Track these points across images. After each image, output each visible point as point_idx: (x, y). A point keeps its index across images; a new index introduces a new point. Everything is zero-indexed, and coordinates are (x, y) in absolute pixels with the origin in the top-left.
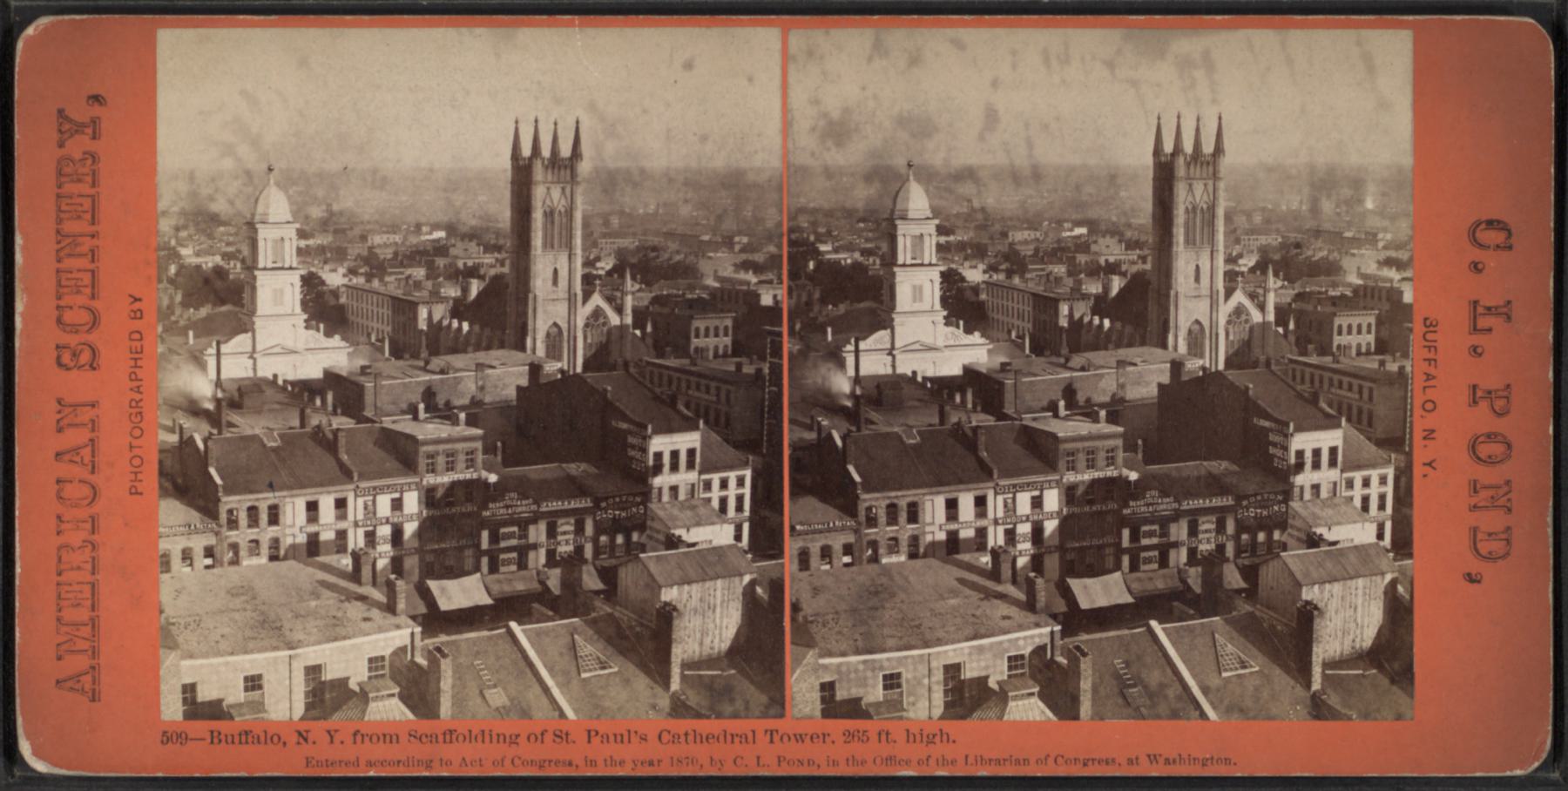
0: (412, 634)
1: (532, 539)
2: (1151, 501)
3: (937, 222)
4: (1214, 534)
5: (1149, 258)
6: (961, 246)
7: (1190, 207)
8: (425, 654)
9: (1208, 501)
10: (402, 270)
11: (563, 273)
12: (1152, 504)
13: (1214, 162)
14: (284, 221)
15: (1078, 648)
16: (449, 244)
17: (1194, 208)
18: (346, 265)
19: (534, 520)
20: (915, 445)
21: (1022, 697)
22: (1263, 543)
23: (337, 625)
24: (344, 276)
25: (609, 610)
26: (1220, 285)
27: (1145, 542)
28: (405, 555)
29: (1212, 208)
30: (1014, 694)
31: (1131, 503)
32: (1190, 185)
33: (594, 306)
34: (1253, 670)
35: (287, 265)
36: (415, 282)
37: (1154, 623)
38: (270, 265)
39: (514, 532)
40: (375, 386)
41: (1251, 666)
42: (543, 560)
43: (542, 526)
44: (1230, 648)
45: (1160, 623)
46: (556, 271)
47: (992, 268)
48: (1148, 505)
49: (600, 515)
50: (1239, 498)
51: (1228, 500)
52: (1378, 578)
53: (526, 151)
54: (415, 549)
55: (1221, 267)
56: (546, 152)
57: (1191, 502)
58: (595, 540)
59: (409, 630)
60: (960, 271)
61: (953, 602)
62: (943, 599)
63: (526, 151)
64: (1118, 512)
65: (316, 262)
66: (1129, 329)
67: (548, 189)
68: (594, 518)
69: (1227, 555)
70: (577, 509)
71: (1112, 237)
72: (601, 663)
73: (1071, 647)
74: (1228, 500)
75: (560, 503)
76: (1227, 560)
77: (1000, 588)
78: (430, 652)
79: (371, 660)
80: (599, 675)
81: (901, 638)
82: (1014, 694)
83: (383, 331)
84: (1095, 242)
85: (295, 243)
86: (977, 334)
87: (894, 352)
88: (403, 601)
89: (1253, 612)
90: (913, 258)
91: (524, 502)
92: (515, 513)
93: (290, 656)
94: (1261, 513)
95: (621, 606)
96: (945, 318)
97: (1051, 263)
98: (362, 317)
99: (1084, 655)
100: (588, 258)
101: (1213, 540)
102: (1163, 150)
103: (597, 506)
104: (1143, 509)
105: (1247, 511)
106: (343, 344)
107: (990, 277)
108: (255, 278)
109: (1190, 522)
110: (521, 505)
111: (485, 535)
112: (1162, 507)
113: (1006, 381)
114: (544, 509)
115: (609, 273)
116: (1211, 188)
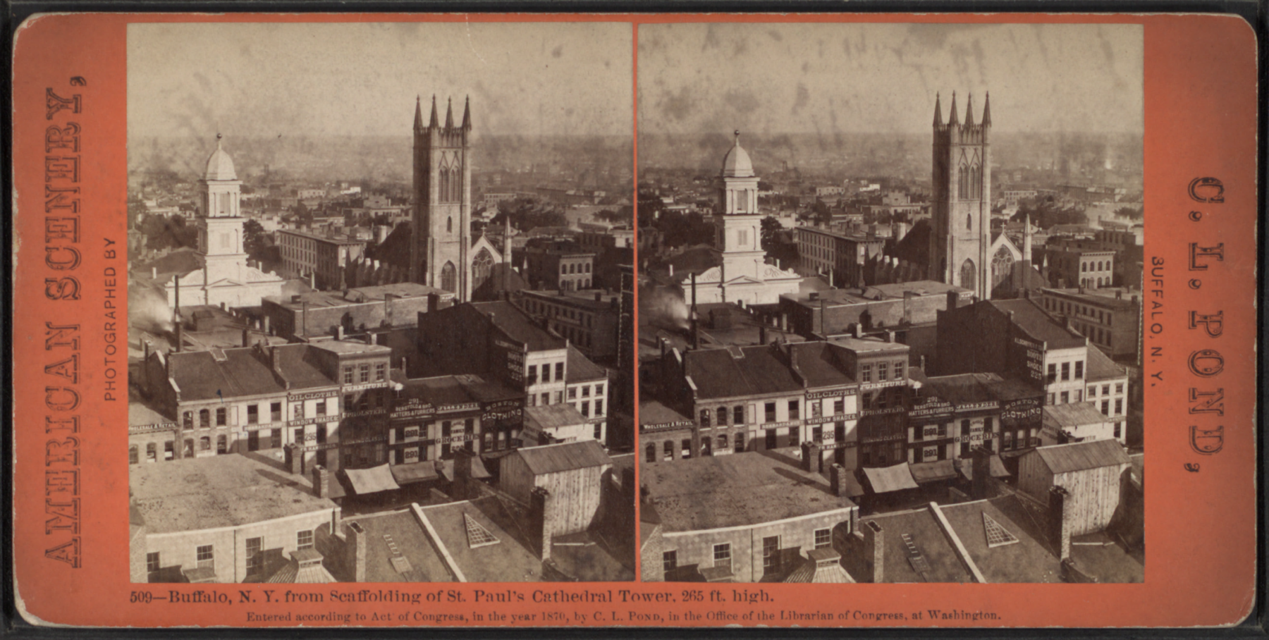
1: (430, 436)
2: (931, 405)
3: (758, 179)
4: (982, 432)
5: (930, 209)
6: (778, 199)
7: (963, 168)
10: (325, 218)
12: (932, 408)
13: (983, 131)
17: (966, 169)
18: (280, 214)
19: (432, 421)
21: (827, 564)
22: (1022, 440)
23: (273, 506)
24: (279, 223)
26: (987, 231)
27: (927, 438)
28: (328, 449)
31: (916, 407)
33: (481, 247)
34: (1014, 542)
36: (336, 228)
37: (934, 504)
38: (218, 214)
40: (304, 312)
42: (439, 453)
43: (439, 426)
44: (995, 524)
45: (939, 504)
46: (450, 219)
48: (929, 408)
49: (486, 417)
50: (1003, 403)
53: (426, 122)
55: (988, 216)
56: (442, 123)
58: (482, 437)
59: (331, 510)
61: (771, 487)
62: (764, 485)
63: (426, 122)
65: (256, 212)
66: (913, 266)
67: (444, 153)
69: (993, 449)
71: (900, 192)
72: (486, 536)
73: (867, 523)
77: (809, 476)
79: (300, 534)
80: (485, 547)
81: (729, 516)
85: (239, 197)
86: (791, 270)
87: (724, 285)
88: (327, 486)
90: (739, 209)
91: (424, 406)
93: (235, 531)
94: (1021, 415)
95: (502, 490)
96: (765, 257)
97: (851, 213)
99: (878, 530)
100: (476, 209)
101: (982, 437)
104: (925, 412)
106: (795, 276)
107: (802, 224)
111: (393, 432)
112: (940, 410)
114: (440, 412)
116: (980, 153)
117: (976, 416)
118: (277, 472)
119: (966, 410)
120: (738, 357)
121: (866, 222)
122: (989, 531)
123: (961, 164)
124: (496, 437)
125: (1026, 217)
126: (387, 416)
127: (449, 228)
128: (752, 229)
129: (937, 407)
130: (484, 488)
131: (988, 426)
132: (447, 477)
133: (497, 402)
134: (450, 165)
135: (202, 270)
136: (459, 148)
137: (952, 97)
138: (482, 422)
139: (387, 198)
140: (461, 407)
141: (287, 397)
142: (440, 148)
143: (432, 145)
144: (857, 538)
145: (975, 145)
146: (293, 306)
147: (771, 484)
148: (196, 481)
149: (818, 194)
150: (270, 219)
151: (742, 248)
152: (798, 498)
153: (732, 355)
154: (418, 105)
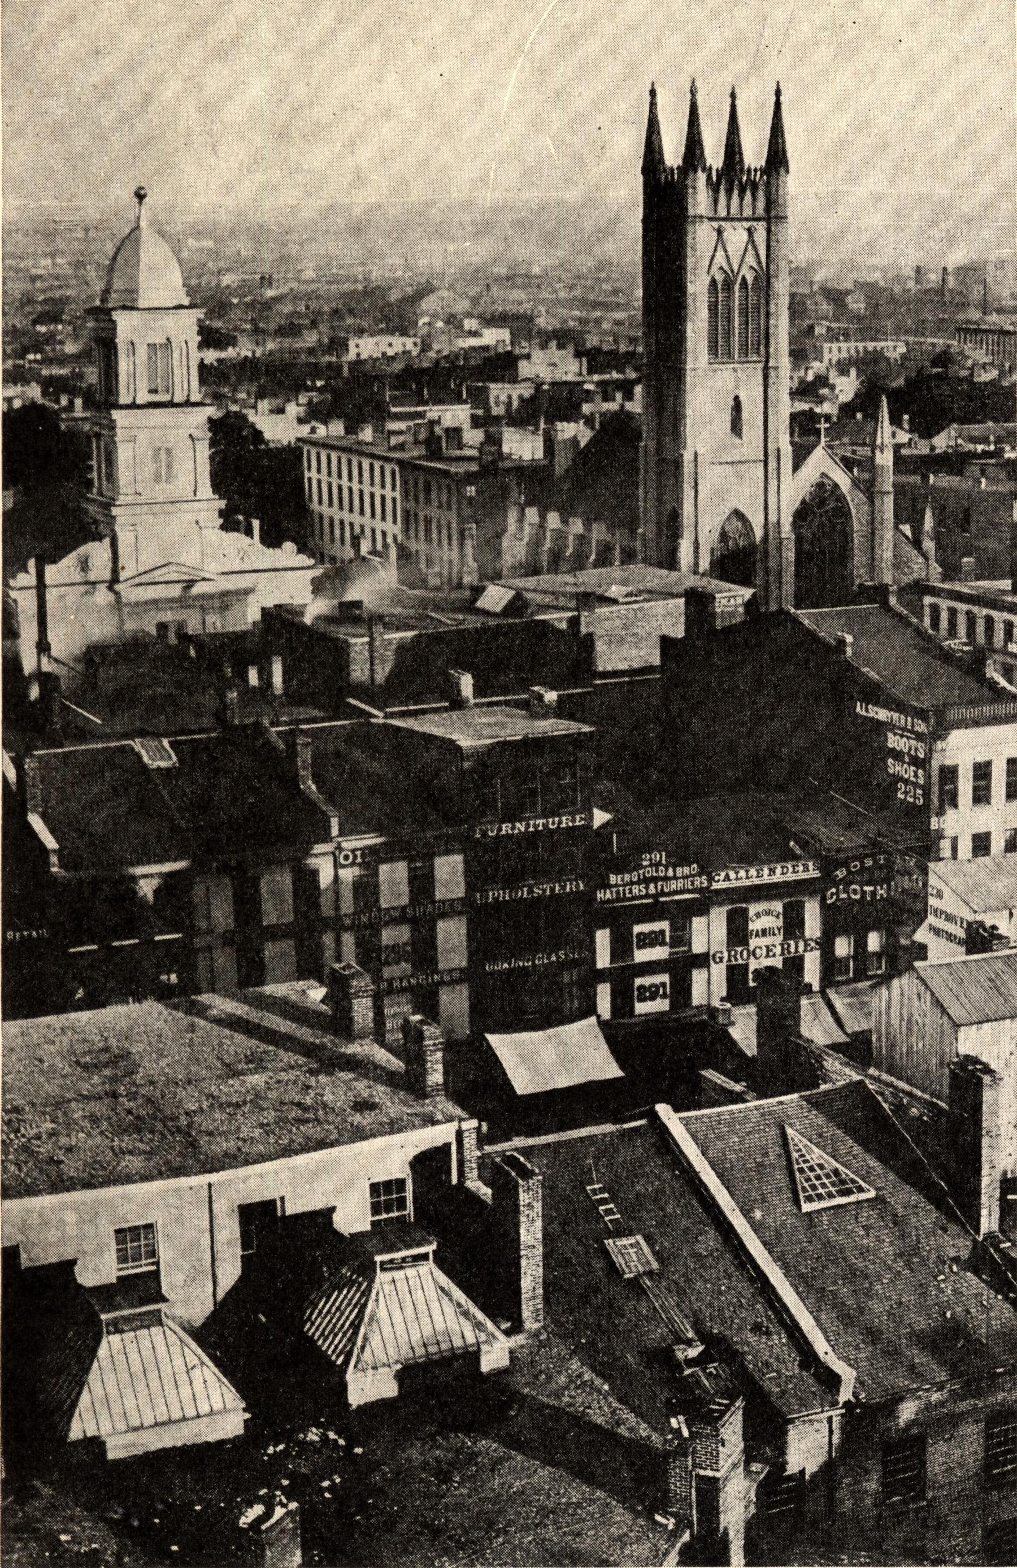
0: (459, 1134)
1: (698, 947)
2: (651, 872)
3: (199, 313)
4: (779, 938)
5: (638, 389)
6: (247, 368)
7: (719, 278)
8: (487, 1174)
9: (753, 872)
10: (420, 409)
11: (753, 416)
12: (655, 880)
13: (768, 184)
14: (171, 305)
15: (512, 1161)
16: (517, 351)
17: (728, 285)
18: (303, 399)
19: (702, 906)
20: (168, 770)
21: (399, 1265)
22: (878, 955)
23: (307, 1121)
24: (301, 421)
25: (856, 1077)
26: (784, 442)
27: (641, 956)
28: (442, 983)
29: (764, 281)
30: (386, 1257)
31: (613, 879)
32: (720, 232)
33: (815, 478)
34: (862, 1196)
35: (178, 398)
36: (447, 430)
37: (663, 1110)
38: (143, 397)
39: (662, 932)
40: (371, 644)
41: (861, 1190)
42: (720, 988)
43: (719, 915)
44: (816, 1155)
45: (676, 1110)
46: (737, 406)
47: (315, 414)
48: (646, 881)
49: (832, 895)
50: (827, 865)
51: (806, 869)
52: (563, 1037)
53: (673, 154)
54: (462, 970)
55: (784, 407)
56: (714, 155)
57: (732, 875)
58: (826, 946)
59: (453, 1126)
60: (252, 418)
61: (256, 1079)
62: (237, 1074)
63: (673, 154)
64: (588, 898)
65: (242, 396)
66: (599, 532)
67: (720, 232)
68: (823, 899)
69: (807, 979)
70: (786, 884)
71: (561, 347)
72: (843, 1182)
73: (498, 1160)
74: (806, 869)
75: (753, 872)
76: (808, 989)
77: (352, 1049)
78: (497, 1168)
79: (375, 1188)
80: (840, 1206)
81: (149, 1154)
82: (386, 1257)
83: (384, 534)
84: (528, 357)
85: (195, 356)
86: (289, 546)
87: (118, 587)
88: (440, 1067)
89: (861, 1082)
90: (154, 391)
91: (679, 871)
92: (663, 894)
93: (210, 1185)
94: (874, 893)
95: (878, 1067)
96: (222, 513)
97: (440, 402)
98: (331, 504)
99: (526, 1174)
100: (802, 381)
101: (778, 950)
102: (661, 161)
103: (827, 878)
104: (635, 890)
105: (846, 891)
106: (304, 560)
107: (313, 430)
108: (112, 426)
109: (731, 917)
110: (675, 878)
111: (603, 938)
112: (673, 885)
113: (353, 641)
114: (719, 885)
115: (847, 410)
116: (760, 237)
117: (758, 899)
118: (304, 1033)
119: (748, 883)
120: (163, 764)
121: (476, 422)
122: (801, 1171)
123: (714, 269)
124: (860, 944)
125: (877, 406)
126: (588, 898)
127: (736, 427)
128: (189, 442)
129: (666, 879)
130: (832, 1064)
131: (793, 926)
132: (743, 1045)
133: (861, 858)
134: (735, 268)
135: (107, 541)
136: (758, 219)
137: (729, 101)
138: (824, 906)
139: (578, 355)
140: (772, 871)
141: (333, 854)
142: (710, 219)
143: (691, 212)
144: (474, 1198)
145: (747, 219)
146: (341, 632)
147: (255, 1071)
148: (106, 1065)
149: (352, 356)
150: (280, 411)
151: (162, 492)
152: (325, 1105)
153: (146, 759)
154: (778, 105)
